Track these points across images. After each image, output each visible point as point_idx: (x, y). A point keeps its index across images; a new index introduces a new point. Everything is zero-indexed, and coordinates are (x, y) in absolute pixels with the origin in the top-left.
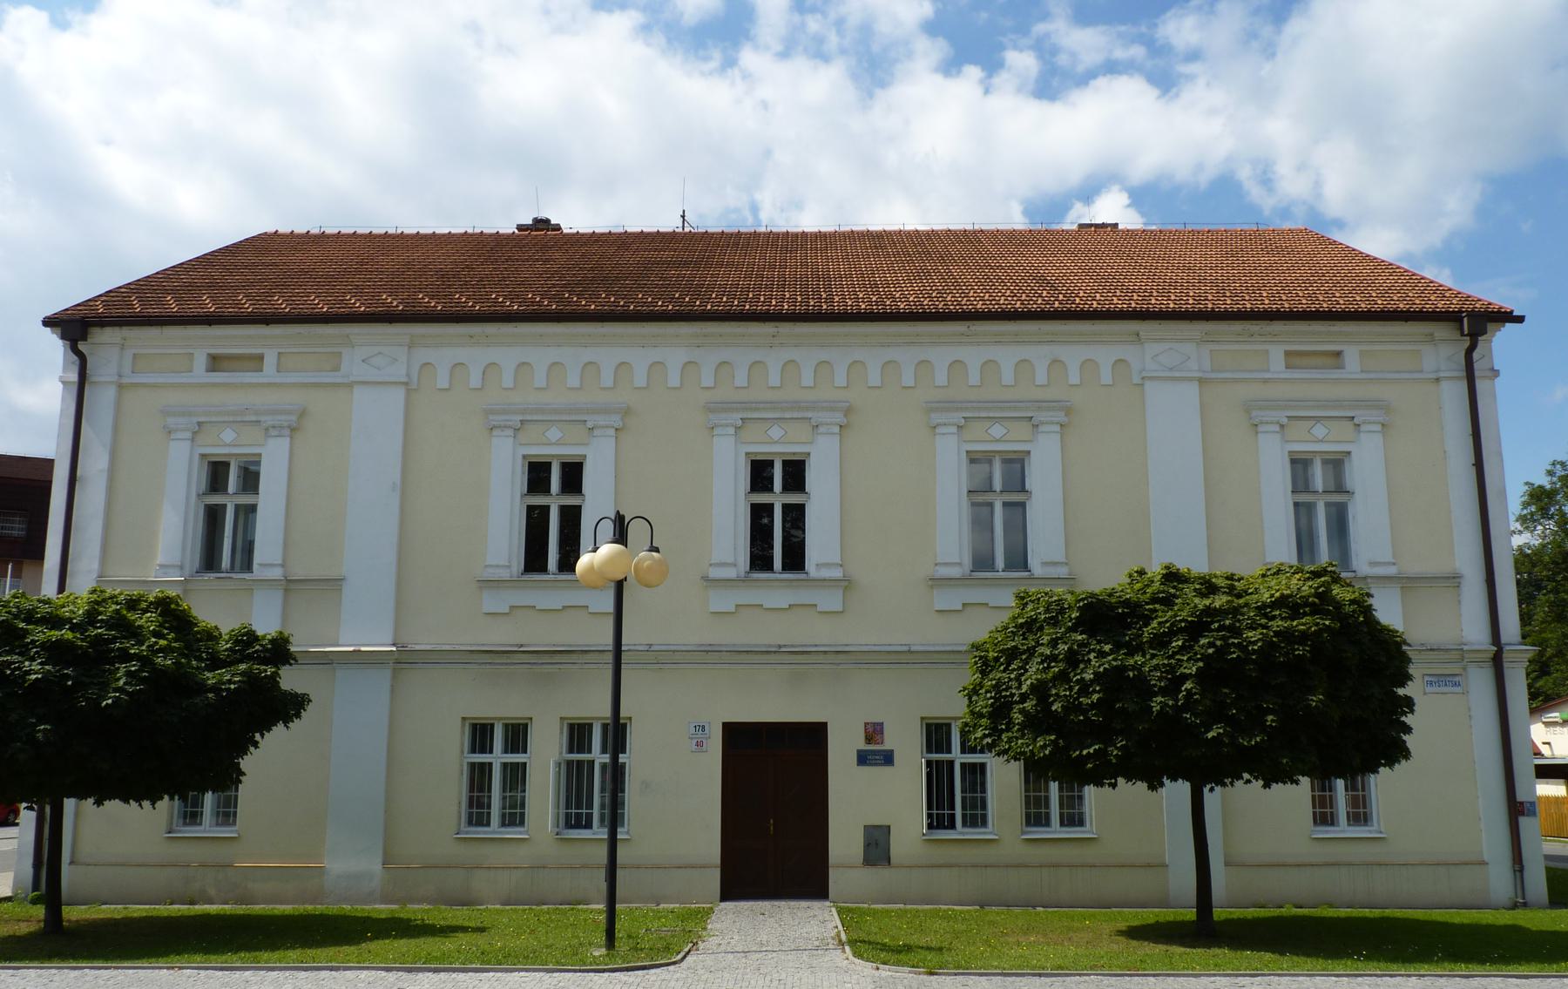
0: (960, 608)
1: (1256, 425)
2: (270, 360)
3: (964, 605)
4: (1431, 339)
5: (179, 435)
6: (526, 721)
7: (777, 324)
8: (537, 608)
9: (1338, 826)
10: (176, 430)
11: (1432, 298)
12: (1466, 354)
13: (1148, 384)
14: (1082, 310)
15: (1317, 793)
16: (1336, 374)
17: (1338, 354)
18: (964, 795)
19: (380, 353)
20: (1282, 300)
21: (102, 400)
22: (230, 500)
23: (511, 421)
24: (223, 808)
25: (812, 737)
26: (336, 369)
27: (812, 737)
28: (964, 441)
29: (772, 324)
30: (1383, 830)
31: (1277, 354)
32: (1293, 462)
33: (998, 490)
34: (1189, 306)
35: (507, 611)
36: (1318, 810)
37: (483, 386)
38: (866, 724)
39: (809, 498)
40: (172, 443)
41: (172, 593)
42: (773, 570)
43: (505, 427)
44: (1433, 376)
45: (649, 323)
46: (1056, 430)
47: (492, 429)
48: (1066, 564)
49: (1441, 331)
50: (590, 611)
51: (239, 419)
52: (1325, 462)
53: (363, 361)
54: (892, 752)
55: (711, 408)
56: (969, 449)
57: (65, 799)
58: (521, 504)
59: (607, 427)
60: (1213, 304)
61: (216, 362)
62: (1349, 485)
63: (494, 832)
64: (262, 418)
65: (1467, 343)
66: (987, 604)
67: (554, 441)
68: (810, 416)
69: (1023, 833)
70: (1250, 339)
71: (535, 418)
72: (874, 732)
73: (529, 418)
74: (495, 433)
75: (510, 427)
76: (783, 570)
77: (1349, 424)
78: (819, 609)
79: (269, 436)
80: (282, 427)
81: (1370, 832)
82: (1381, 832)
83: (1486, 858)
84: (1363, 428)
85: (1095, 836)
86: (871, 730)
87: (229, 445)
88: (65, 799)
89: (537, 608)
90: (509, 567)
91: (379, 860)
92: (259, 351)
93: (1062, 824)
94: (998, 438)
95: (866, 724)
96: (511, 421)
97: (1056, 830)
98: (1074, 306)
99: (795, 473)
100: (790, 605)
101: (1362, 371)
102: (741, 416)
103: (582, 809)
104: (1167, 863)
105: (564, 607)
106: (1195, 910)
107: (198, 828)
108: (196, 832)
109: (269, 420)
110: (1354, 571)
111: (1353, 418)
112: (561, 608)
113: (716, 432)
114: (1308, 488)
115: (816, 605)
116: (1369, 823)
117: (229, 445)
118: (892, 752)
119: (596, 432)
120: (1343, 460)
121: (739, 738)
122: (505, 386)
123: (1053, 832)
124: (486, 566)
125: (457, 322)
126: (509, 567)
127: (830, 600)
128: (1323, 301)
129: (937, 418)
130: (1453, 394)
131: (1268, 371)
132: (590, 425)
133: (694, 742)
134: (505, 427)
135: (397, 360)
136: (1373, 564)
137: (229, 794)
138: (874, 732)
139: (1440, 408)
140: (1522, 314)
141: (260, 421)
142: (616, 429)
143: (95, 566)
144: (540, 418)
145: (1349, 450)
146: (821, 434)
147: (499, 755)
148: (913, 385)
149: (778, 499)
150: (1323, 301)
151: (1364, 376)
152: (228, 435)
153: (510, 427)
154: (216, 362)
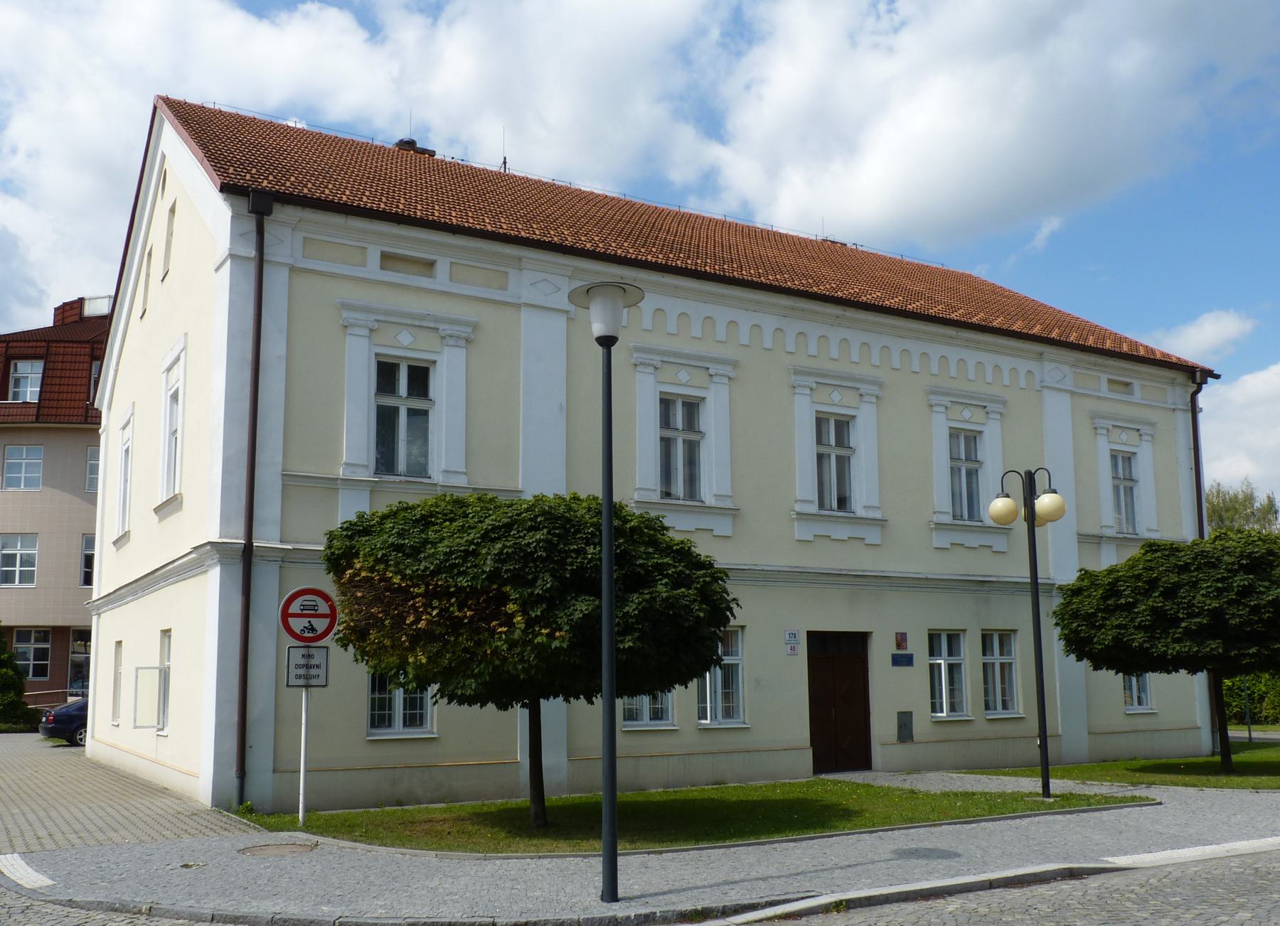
1: (794, 387)
2: (442, 267)
4: (1172, 382)
5: (357, 331)
6: (736, 629)
7: (958, 329)
9: (642, 720)
10: (353, 325)
11: (566, 233)
12: (1191, 396)
13: (1046, 393)
14: (291, 194)
15: (377, 695)
16: (423, 282)
17: (1127, 384)
18: (406, 696)
19: (546, 280)
20: (485, 222)
21: (277, 280)
22: (402, 401)
23: (655, 360)
24: (385, 714)
25: (859, 641)
26: (504, 288)
27: (859, 641)
29: (842, 308)
30: (675, 724)
31: (1104, 378)
32: (662, 401)
34: (374, 205)
36: (418, 711)
38: (897, 633)
39: (854, 453)
40: (934, 414)
41: (653, 514)
43: (648, 365)
44: (1173, 407)
46: (363, 334)
48: (465, 473)
49: (1180, 377)
50: (994, 550)
51: (417, 323)
52: (684, 404)
53: (531, 284)
54: (912, 655)
55: (934, 392)
56: (662, 390)
57: (541, 700)
60: (440, 214)
61: (388, 259)
62: (1135, 476)
63: (647, 725)
64: (441, 327)
65: (1194, 387)
69: (368, 735)
70: (1094, 368)
72: (901, 640)
77: (1136, 434)
80: (458, 337)
81: (738, 723)
82: (674, 725)
83: (1199, 725)
84: (1143, 438)
85: (437, 736)
86: (899, 638)
87: (406, 348)
88: (541, 700)
91: (565, 754)
92: (432, 257)
93: (405, 725)
94: (836, 402)
95: (897, 633)
97: (398, 730)
98: (283, 188)
99: (420, 378)
101: (1142, 399)
103: (379, 714)
104: (1060, 732)
106: (1040, 767)
107: (635, 723)
108: (387, 734)
109: (445, 329)
110: (853, 512)
111: (708, 369)
113: (349, 331)
114: (669, 426)
116: (424, 726)
117: (406, 348)
118: (912, 655)
120: (399, 364)
121: (818, 641)
122: (988, 381)
123: (998, 714)
125: (564, 254)
127: (872, 536)
128: (522, 229)
129: (935, 399)
130: (1183, 419)
131: (1100, 391)
133: (789, 646)
134: (648, 365)
135: (560, 289)
136: (1149, 530)
137: (385, 696)
138: (901, 640)
139: (1175, 429)
140: (1219, 374)
141: (438, 329)
143: (279, 458)
145: (1135, 451)
146: (865, 402)
147: (999, 657)
149: (402, 401)
150: (522, 229)
151: (1143, 402)
152: (405, 338)
153: (652, 365)
154: (388, 259)
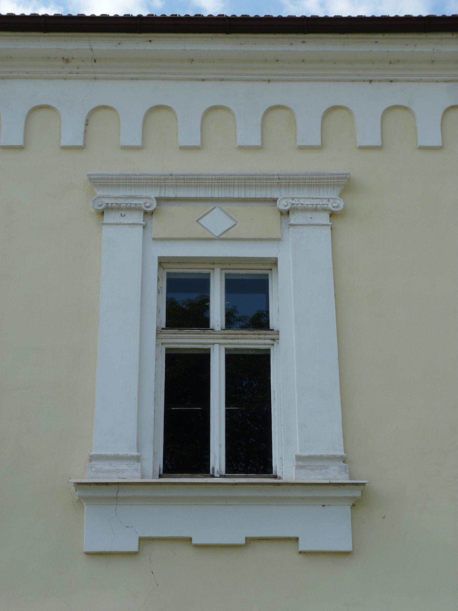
0: (243, 541)
3: (142, 540)
8: (194, 542)
23: (140, 198)
28: (154, 239)
33: (218, 328)
35: (134, 547)
37: (84, 144)
40: (104, 228)
42: (208, 471)
45: (387, 36)
47: (102, 213)
58: (157, 345)
59: (316, 210)
66: (190, 539)
67: (217, 233)
68: (275, 196)
71: (182, 193)
73: (170, 193)
74: (109, 218)
75: (136, 209)
76: (227, 472)
78: (303, 546)
79: (103, 224)
89: (194, 542)
90: (138, 459)
96: (140, 198)
100: (247, 539)
102: (157, 195)
105: (249, 540)
112: (243, 541)
115: (297, 539)
117: (219, 239)
119: (293, 219)
124: (93, 458)
125: (228, 33)
126: (138, 459)
132: (283, 205)
142: (146, 213)
144: (193, 193)
148: (198, 143)
153: (136, 209)
